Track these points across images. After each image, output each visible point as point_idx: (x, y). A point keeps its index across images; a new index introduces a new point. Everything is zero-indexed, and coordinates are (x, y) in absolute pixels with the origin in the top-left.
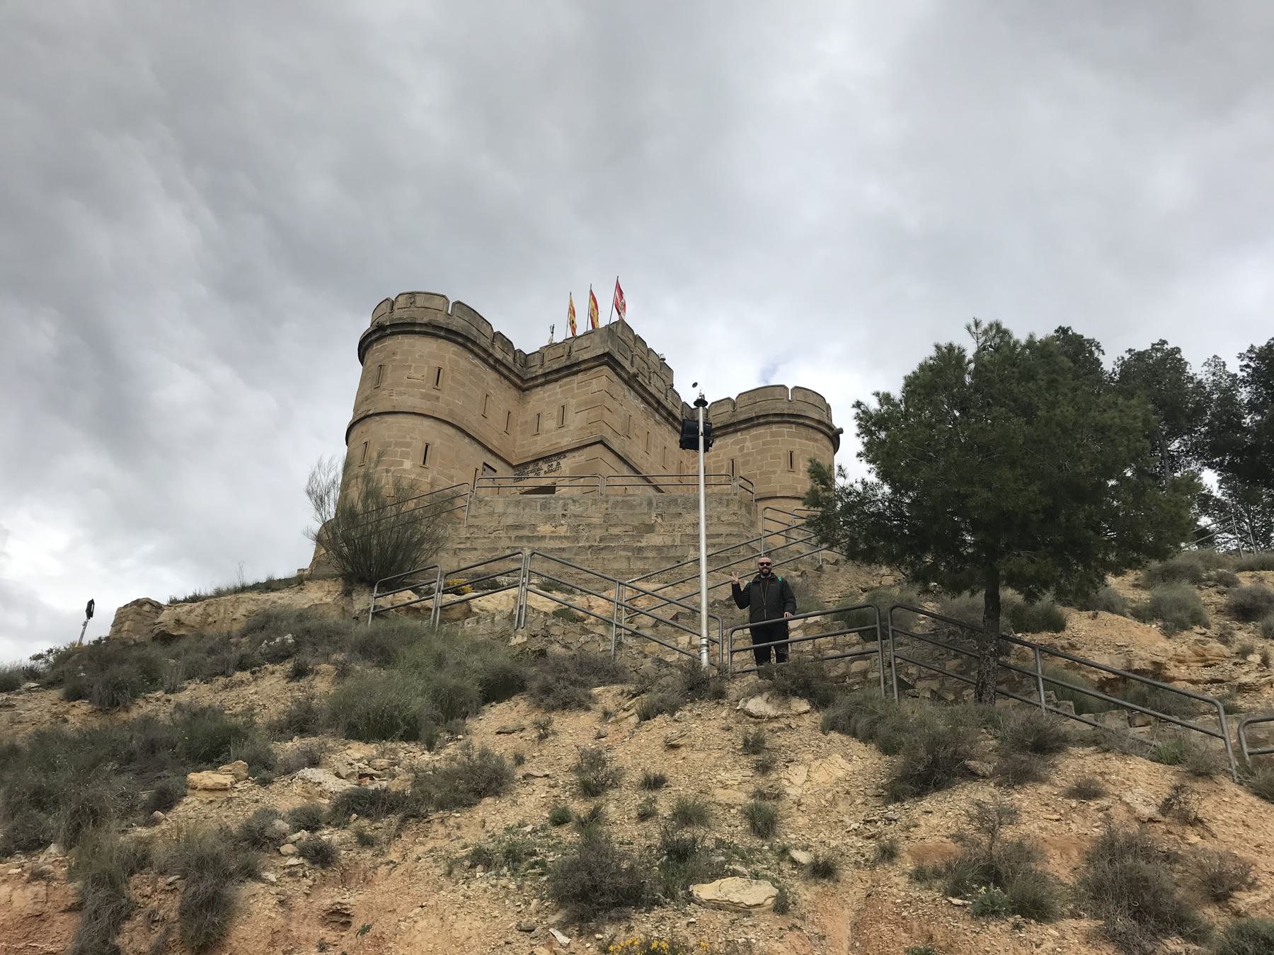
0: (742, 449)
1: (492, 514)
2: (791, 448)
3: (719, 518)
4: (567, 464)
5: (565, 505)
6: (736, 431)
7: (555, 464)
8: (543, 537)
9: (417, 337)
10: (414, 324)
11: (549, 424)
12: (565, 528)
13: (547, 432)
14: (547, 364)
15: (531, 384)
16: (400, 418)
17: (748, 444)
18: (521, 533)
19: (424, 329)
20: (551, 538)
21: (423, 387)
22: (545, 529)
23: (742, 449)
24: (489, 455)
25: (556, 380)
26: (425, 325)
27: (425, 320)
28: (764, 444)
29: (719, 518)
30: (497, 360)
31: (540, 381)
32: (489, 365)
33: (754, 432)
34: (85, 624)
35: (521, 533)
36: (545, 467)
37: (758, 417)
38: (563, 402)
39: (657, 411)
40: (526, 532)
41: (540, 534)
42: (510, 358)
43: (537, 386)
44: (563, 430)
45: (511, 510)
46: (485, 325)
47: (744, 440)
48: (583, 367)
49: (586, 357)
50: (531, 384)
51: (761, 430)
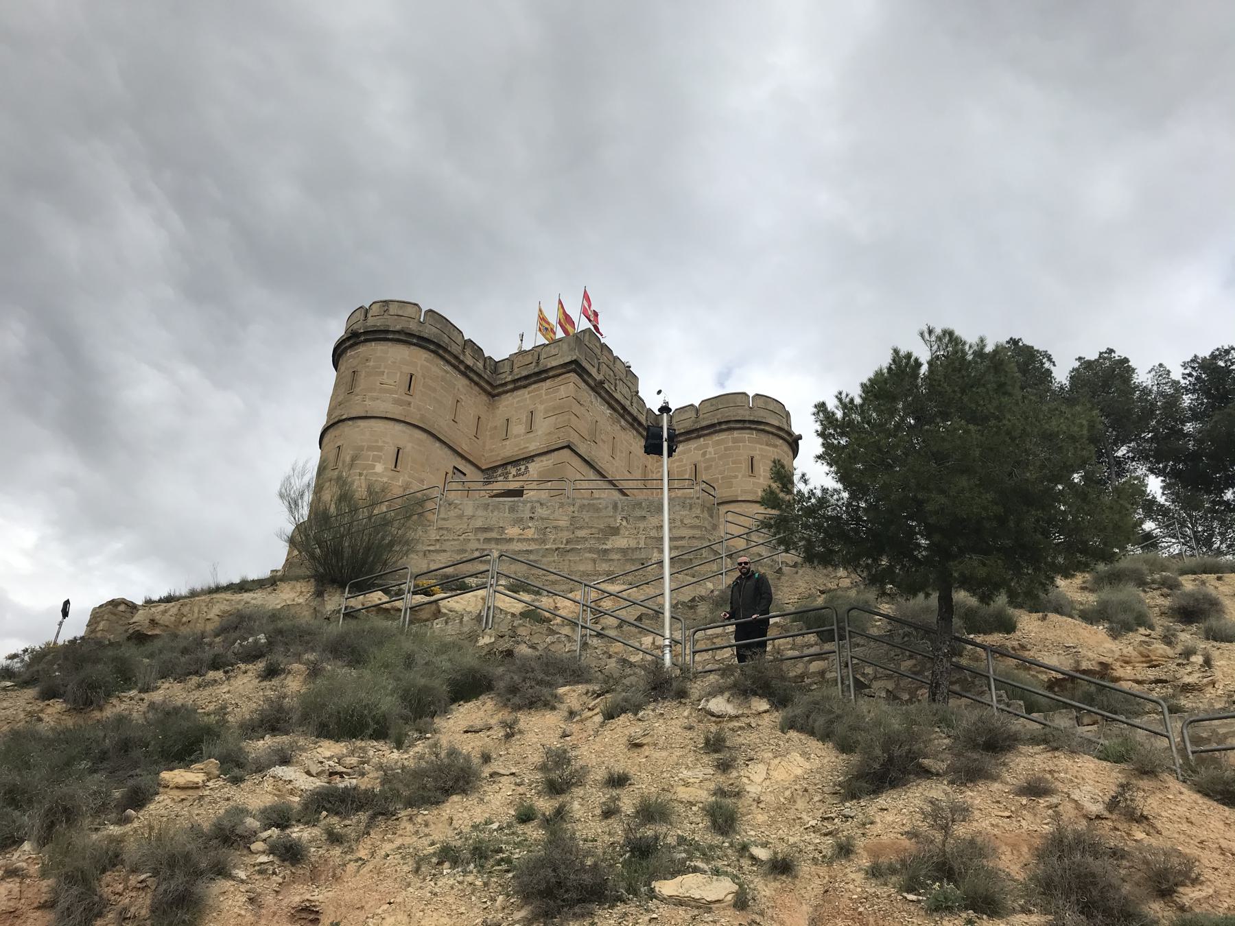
2: (752, 453)
3: (682, 521)
4: (534, 468)
5: (533, 508)
6: (699, 437)
7: (523, 468)
8: (511, 540)
9: (390, 344)
10: (387, 332)
11: (518, 429)
13: (516, 437)
14: (516, 370)
15: (501, 390)
16: (372, 422)
18: (488, 535)
19: (397, 336)
20: (519, 540)
22: (513, 531)
23: (704, 454)
25: (525, 387)
26: (398, 332)
27: (398, 328)
30: (467, 367)
31: (509, 387)
33: (716, 437)
34: (61, 624)
35: (488, 535)
36: (513, 471)
37: (720, 423)
38: (531, 407)
39: (623, 417)
40: (494, 535)
42: (480, 365)
43: (507, 392)
44: (531, 435)
46: (456, 333)
47: (707, 446)
49: (554, 364)
50: (501, 390)
51: (723, 436)
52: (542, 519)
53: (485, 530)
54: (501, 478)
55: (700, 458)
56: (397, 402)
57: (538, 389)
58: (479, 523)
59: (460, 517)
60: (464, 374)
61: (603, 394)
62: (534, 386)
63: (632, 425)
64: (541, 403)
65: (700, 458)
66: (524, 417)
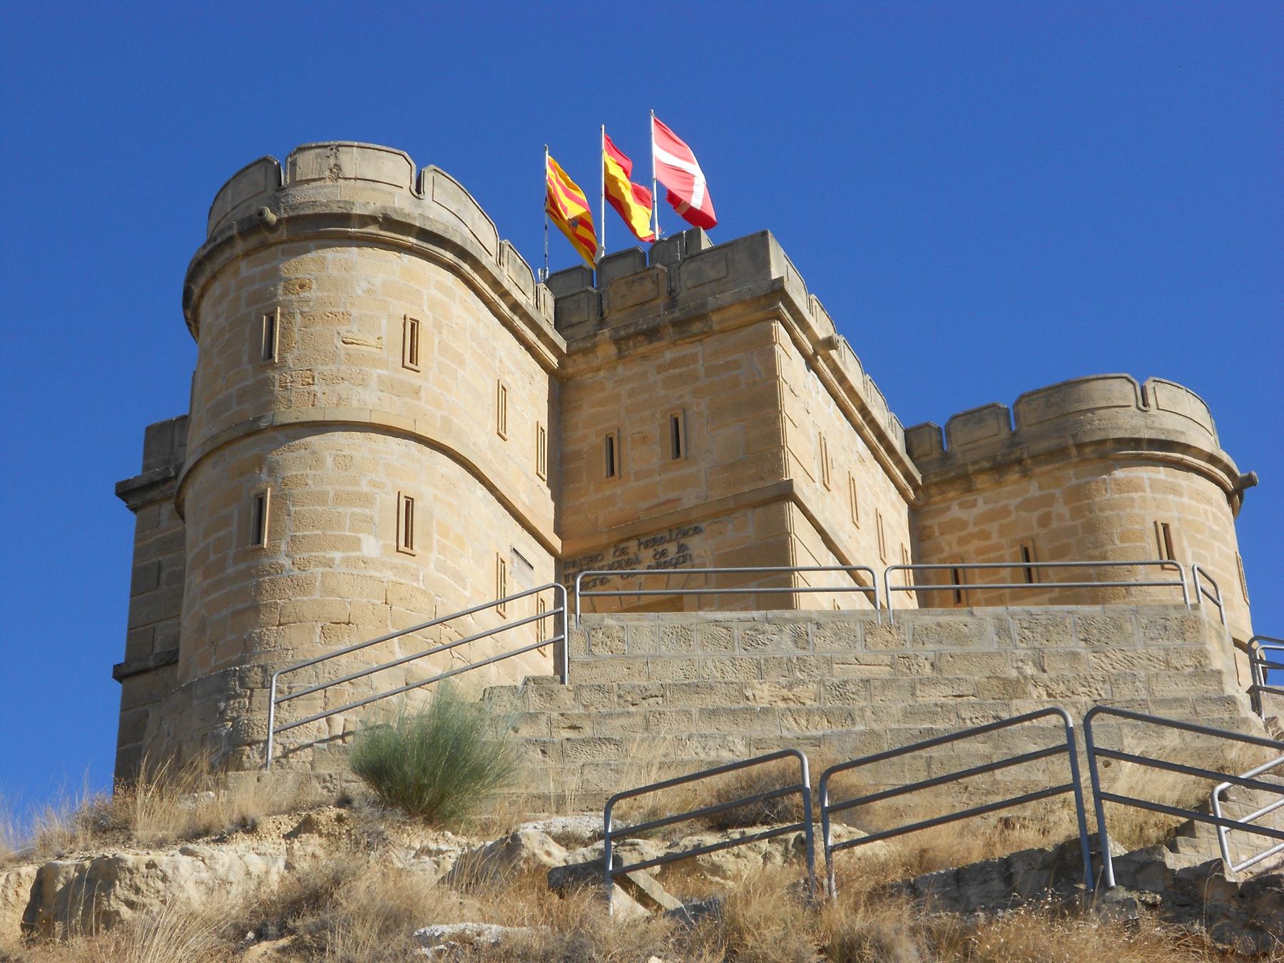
7: (672, 549)
23: (1044, 521)
47: (1050, 500)
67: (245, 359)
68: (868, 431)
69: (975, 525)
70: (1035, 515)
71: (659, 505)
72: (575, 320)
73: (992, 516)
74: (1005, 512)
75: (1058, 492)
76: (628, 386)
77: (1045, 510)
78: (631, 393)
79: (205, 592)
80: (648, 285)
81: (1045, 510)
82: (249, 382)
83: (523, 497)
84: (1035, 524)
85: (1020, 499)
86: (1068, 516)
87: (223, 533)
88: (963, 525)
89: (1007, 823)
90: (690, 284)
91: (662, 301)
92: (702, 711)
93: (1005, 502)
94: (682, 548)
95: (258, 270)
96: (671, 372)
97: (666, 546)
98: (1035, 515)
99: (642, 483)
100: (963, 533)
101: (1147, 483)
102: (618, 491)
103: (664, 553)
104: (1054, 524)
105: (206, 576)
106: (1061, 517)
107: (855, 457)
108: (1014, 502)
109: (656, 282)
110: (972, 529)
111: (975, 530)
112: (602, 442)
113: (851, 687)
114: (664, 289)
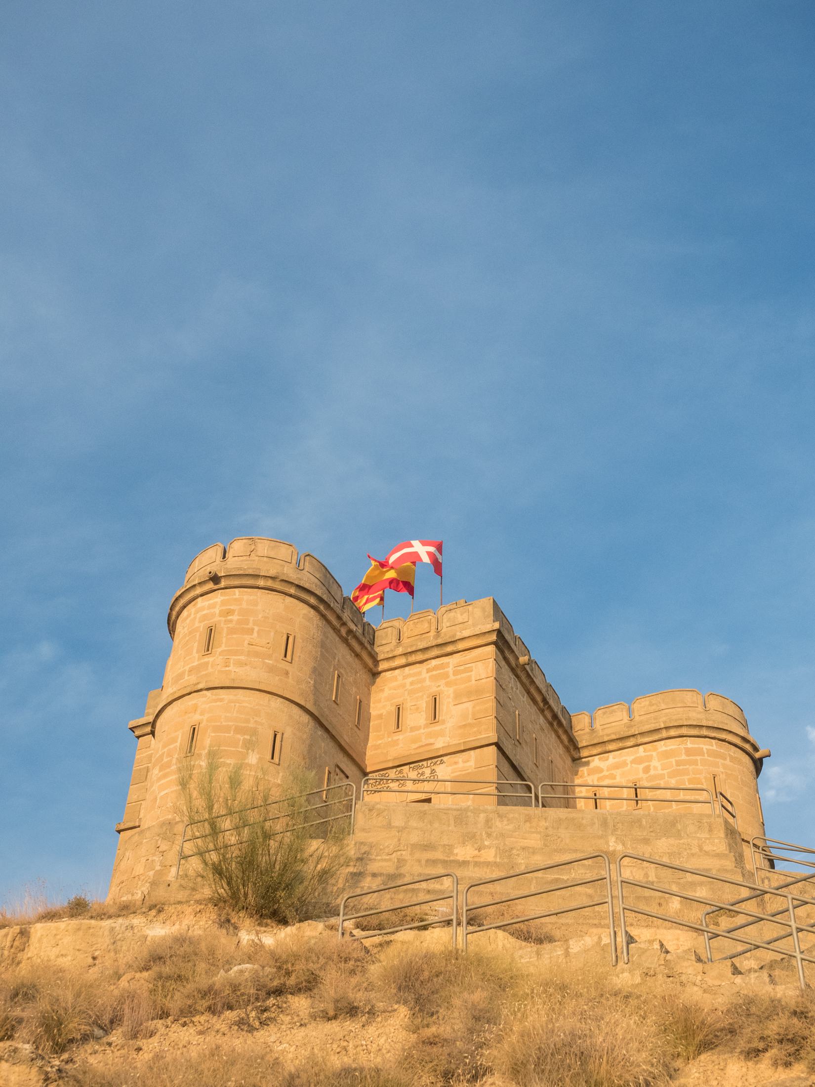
0: (647, 770)
1: (389, 826)
2: (714, 770)
3: (701, 850)
4: (444, 771)
5: (488, 821)
7: (428, 772)
8: (465, 863)
11: (416, 718)
12: (492, 851)
13: (413, 729)
14: (405, 641)
17: (655, 763)
18: (430, 855)
19: (270, 583)
20: (477, 864)
21: (270, 657)
22: (464, 852)
23: (647, 770)
24: (345, 759)
26: (273, 578)
27: (272, 572)
28: (678, 763)
29: (701, 850)
30: (350, 632)
32: (341, 637)
33: (662, 746)
35: (430, 855)
38: (434, 690)
39: (542, 711)
40: (439, 855)
41: (460, 858)
42: (360, 631)
44: (437, 728)
45: (413, 823)
46: (335, 586)
47: (649, 758)
48: (461, 646)
49: (466, 633)
51: (671, 745)
52: (502, 835)
53: (428, 847)
54: (394, 786)
55: (641, 775)
56: (271, 669)
57: (442, 666)
58: (414, 838)
59: (389, 826)
60: (345, 641)
61: (523, 677)
62: (434, 662)
63: (551, 724)
64: (448, 684)
65: (641, 775)
66: (424, 703)
67: (195, 651)
68: (611, 747)
69: (608, 771)
70: (641, 766)
71: (422, 746)
72: (384, 642)
73: (617, 766)
74: (624, 764)
75: (654, 754)
76: (411, 679)
77: (647, 764)
78: (412, 683)
79: (159, 779)
80: (426, 625)
81: (647, 764)
82: (196, 663)
83: (345, 737)
84: (641, 771)
85: (633, 757)
86: (659, 768)
87: (172, 746)
88: (601, 770)
89: (509, 906)
90: (448, 624)
91: (432, 633)
92: (427, 861)
93: (624, 758)
94: (433, 772)
95: (207, 603)
96: (434, 673)
97: (424, 770)
98: (641, 766)
99: (413, 734)
100: (601, 775)
101: (705, 751)
102: (401, 737)
103: (422, 774)
104: (652, 772)
105: (160, 771)
106: (655, 768)
107: (538, 726)
108: (629, 759)
109: (430, 622)
110: (606, 773)
111: (607, 773)
112: (394, 709)
113: (514, 851)
114: (433, 628)
